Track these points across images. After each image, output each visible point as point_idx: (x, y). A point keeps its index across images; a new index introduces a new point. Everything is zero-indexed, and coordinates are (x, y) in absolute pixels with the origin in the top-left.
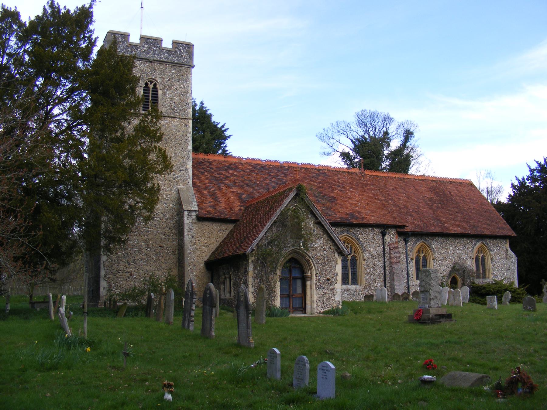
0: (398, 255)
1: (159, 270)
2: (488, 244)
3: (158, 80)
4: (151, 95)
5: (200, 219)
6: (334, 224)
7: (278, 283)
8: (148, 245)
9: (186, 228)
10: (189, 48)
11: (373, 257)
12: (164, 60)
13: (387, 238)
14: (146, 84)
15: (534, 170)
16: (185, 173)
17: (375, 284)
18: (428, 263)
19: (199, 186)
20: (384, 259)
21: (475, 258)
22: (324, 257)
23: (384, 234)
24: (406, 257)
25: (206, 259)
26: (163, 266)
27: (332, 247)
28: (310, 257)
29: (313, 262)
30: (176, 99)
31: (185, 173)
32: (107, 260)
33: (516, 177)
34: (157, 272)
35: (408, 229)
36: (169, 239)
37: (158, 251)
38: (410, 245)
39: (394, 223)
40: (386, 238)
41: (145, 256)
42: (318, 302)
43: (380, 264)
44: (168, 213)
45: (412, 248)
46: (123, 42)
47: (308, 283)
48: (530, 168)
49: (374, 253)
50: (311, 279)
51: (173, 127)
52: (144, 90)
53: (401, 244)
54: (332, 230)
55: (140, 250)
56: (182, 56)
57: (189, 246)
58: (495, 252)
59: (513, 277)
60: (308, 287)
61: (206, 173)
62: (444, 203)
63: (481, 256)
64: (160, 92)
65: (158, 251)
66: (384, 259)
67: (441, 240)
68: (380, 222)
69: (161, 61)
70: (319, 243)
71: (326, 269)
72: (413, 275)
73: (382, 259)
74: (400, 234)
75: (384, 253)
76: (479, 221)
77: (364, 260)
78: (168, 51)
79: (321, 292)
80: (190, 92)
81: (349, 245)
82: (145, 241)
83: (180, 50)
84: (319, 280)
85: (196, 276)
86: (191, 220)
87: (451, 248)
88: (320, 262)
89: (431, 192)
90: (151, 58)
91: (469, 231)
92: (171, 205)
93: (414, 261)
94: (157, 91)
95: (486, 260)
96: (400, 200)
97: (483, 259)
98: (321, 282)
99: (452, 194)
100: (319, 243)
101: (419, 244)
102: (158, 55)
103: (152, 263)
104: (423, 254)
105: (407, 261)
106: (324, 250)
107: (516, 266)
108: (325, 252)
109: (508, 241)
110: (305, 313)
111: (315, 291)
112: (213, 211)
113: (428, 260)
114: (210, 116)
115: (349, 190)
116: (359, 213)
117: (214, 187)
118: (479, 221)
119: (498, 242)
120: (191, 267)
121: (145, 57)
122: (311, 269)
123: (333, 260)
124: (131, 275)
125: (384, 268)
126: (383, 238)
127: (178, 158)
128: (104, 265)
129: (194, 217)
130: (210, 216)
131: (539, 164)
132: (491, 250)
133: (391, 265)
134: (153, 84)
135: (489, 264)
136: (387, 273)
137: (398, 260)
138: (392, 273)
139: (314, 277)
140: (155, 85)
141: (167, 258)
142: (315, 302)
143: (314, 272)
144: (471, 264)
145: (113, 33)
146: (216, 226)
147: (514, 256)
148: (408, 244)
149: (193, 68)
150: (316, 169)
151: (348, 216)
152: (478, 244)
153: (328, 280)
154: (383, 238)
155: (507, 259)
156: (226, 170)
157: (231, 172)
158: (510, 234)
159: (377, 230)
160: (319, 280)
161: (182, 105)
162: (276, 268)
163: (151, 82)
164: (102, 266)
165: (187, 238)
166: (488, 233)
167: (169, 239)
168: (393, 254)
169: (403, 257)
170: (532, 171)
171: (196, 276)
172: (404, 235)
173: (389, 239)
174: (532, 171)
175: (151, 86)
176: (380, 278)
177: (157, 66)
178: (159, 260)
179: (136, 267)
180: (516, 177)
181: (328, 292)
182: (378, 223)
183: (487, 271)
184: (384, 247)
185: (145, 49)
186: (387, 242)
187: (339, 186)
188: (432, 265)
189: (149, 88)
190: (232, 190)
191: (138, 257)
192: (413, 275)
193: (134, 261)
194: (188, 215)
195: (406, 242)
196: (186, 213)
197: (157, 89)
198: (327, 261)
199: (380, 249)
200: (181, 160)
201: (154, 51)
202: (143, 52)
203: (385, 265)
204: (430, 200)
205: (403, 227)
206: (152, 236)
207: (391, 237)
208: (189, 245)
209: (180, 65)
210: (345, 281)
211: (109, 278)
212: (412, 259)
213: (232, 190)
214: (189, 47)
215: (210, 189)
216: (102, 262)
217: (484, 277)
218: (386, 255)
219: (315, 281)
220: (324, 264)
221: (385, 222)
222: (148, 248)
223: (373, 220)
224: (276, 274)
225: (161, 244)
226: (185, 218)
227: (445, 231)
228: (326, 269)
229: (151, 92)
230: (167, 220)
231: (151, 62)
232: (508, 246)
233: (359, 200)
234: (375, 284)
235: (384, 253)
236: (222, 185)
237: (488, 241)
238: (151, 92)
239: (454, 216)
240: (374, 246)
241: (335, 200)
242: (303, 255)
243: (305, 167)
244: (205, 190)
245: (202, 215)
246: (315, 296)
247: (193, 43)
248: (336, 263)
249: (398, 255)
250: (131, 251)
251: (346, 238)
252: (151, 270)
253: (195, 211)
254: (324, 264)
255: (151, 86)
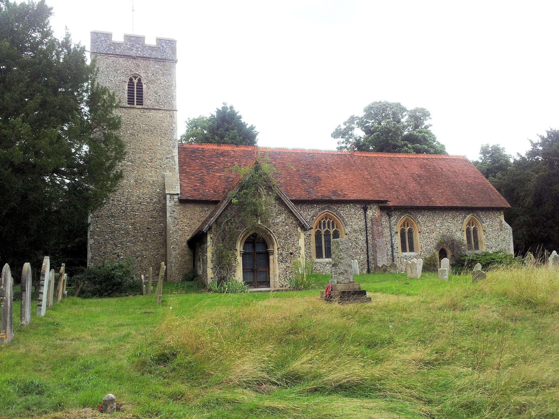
0: (380, 228)
1: (146, 250)
2: (479, 217)
3: (142, 75)
4: (135, 90)
5: (183, 202)
6: (297, 202)
7: (240, 259)
8: (135, 228)
9: (169, 210)
10: (172, 44)
11: (355, 231)
12: (147, 56)
13: (370, 213)
14: (131, 80)
15: (537, 144)
16: (171, 160)
17: (358, 257)
18: (414, 235)
19: (188, 172)
20: (367, 233)
21: (465, 230)
22: (286, 232)
23: (365, 210)
24: (390, 230)
25: (188, 238)
26: (150, 247)
27: (294, 222)
28: (271, 233)
29: (274, 237)
30: (161, 93)
31: (171, 160)
32: (94, 243)
33: (518, 154)
34: (144, 252)
35: (390, 204)
36: (156, 221)
37: (145, 232)
38: (394, 219)
39: (377, 199)
40: (368, 213)
41: (132, 238)
42: (281, 275)
43: (362, 238)
44: (155, 198)
45: (396, 222)
46: (106, 41)
47: (271, 257)
48: (532, 143)
49: (356, 227)
50: (273, 253)
51: (158, 118)
52: (128, 85)
53: (385, 219)
54: (291, 205)
55: (127, 233)
56: (165, 52)
57: (171, 227)
58: (487, 223)
59: (509, 248)
60: (271, 261)
61: (197, 161)
62: (433, 179)
63: (472, 228)
64: (144, 86)
65: (145, 232)
66: (367, 233)
67: (427, 213)
68: (362, 198)
69: (144, 57)
70: (281, 219)
71: (289, 243)
72: (397, 248)
73: (364, 233)
74: (382, 209)
75: (366, 227)
76: (470, 194)
77: (346, 234)
78: (152, 48)
79: (283, 266)
80: (174, 85)
81: (331, 221)
82: (133, 224)
83: (163, 46)
84: (281, 254)
85: (179, 254)
86: (173, 203)
87: (438, 221)
88: (282, 237)
89: (421, 168)
90: (134, 55)
91: (458, 204)
92: (158, 190)
93: (399, 234)
94: (142, 86)
95: (478, 232)
96: (387, 178)
97: (475, 231)
98: (284, 256)
99: (444, 170)
100: (281, 219)
101: (403, 218)
102: (141, 52)
103: (139, 244)
104: (409, 228)
105: (391, 235)
106: (286, 225)
107: (512, 237)
108: (287, 227)
109: (502, 212)
110: (269, 287)
111: (277, 265)
112: (196, 193)
113: (414, 233)
114: (240, 117)
115: (335, 170)
116: (341, 190)
117: (202, 172)
118: (470, 194)
119: (491, 214)
120: (173, 246)
121: (128, 54)
122: (273, 244)
123: (296, 235)
124: (118, 256)
125: (367, 242)
126: (365, 213)
127: (163, 147)
128: (91, 249)
129: (176, 200)
130: (192, 199)
131: (542, 138)
132: (483, 222)
133: (373, 239)
134: (137, 79)
135: (481, 235)
136: (370, 246)
137: (381, 234)
138: (374, 246)
139: (276, 251)
140: (140, 80)
141: (154, 239)
142: (278, 276)
143: (276, 247)
144: (461, 236)
145: (95, 33)
146: (198, 208)
147: (509, 227)
148: (392, 219)
149: (176, 62)
150: (306, 153)
151: (330, 194)
152: (469, 217)
153: (291, 254)
154: (365, 213)
155: (501, 230)
156: (218, 157)
157: (222, 159)
158: (504, 206)
159: (358, 206)
160: (281, 254)
161: (166, 97)
162: (235, 243)
163: (135, 78)
164: (89, 249)
165: (169, 220)
166: (479, 205)
167: (156, 221)
168: (375, 228)
169: (387, 232)
170: (535, 145)
171: (179, 254)
172: (386, 209)
173: (371, 214)
174: (535, 145)
175: (136, 81)
176: (363, 251)
177: (141, 63)
178: (146, 240)
179: (123, 249)
180: (518, 154)
181: (290, 265)
182: (359, 199)
183: (479, 243)
184: (366, 222)
185: (128, 46)
186: (369, 217)
187: (326, 167)
188: (418, 237)
189: (133, 83)
190: (219, 174)
191: (125, 240)
192: (397, 248)
193: (121, 243)
194: (170, 198)
195: (390, 216)
196: (168, 196)
197: (141, 83)
198: (287, 237)
199: (362, 223)
200: (167, 148)
201: (137, 48)
202: (126, 49)
203: (367, 239)
204: (419, 177)
205: (386, 201)
206: (139, 219)
207: (373, 212)
208: (172, 226)
209: (163, 60)
210: (404, 249)
211: (96, 259)
212: (397, 233)
213: (219, 174)
214: (171, 43)
215: (198, 175)
216: (89, 245)
217: (477, 248)
218: (368, 229)
219: (277, 256)
220: (286, 239)
221: (366, 197)
222: (135, 230)
223: (353, 197)
224: (236, 250)
225: (148, 227)
226: (168, 202)
227: (431, 204)
228: (289, 243)
229: (135, 87)
230: (154, 203)
231: (134, 58)
232: (502, 218)
233: (344, 179)
234: (358, 257)
235: (366, 227)
236: (211, 170)
237: (480, 213)
238: (135, 87)
239: (443, 190)
240: (356, 221)
241: (320, 180)
242: (265, 232)
243: (296, 151)
244: (193, 175)
245: (184, 198)
246: (278, 270)
247: (176, 40)
248: (299, 237)
249: (380, 228)
250: (118, 234)
251: (327, 214)
252: (138, 251)
253: (178, 194)
254: (286, 239)
255: (136, 81)
